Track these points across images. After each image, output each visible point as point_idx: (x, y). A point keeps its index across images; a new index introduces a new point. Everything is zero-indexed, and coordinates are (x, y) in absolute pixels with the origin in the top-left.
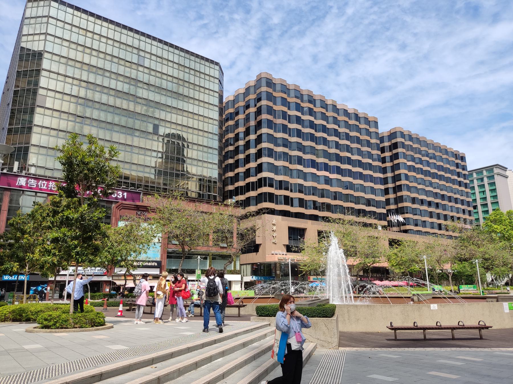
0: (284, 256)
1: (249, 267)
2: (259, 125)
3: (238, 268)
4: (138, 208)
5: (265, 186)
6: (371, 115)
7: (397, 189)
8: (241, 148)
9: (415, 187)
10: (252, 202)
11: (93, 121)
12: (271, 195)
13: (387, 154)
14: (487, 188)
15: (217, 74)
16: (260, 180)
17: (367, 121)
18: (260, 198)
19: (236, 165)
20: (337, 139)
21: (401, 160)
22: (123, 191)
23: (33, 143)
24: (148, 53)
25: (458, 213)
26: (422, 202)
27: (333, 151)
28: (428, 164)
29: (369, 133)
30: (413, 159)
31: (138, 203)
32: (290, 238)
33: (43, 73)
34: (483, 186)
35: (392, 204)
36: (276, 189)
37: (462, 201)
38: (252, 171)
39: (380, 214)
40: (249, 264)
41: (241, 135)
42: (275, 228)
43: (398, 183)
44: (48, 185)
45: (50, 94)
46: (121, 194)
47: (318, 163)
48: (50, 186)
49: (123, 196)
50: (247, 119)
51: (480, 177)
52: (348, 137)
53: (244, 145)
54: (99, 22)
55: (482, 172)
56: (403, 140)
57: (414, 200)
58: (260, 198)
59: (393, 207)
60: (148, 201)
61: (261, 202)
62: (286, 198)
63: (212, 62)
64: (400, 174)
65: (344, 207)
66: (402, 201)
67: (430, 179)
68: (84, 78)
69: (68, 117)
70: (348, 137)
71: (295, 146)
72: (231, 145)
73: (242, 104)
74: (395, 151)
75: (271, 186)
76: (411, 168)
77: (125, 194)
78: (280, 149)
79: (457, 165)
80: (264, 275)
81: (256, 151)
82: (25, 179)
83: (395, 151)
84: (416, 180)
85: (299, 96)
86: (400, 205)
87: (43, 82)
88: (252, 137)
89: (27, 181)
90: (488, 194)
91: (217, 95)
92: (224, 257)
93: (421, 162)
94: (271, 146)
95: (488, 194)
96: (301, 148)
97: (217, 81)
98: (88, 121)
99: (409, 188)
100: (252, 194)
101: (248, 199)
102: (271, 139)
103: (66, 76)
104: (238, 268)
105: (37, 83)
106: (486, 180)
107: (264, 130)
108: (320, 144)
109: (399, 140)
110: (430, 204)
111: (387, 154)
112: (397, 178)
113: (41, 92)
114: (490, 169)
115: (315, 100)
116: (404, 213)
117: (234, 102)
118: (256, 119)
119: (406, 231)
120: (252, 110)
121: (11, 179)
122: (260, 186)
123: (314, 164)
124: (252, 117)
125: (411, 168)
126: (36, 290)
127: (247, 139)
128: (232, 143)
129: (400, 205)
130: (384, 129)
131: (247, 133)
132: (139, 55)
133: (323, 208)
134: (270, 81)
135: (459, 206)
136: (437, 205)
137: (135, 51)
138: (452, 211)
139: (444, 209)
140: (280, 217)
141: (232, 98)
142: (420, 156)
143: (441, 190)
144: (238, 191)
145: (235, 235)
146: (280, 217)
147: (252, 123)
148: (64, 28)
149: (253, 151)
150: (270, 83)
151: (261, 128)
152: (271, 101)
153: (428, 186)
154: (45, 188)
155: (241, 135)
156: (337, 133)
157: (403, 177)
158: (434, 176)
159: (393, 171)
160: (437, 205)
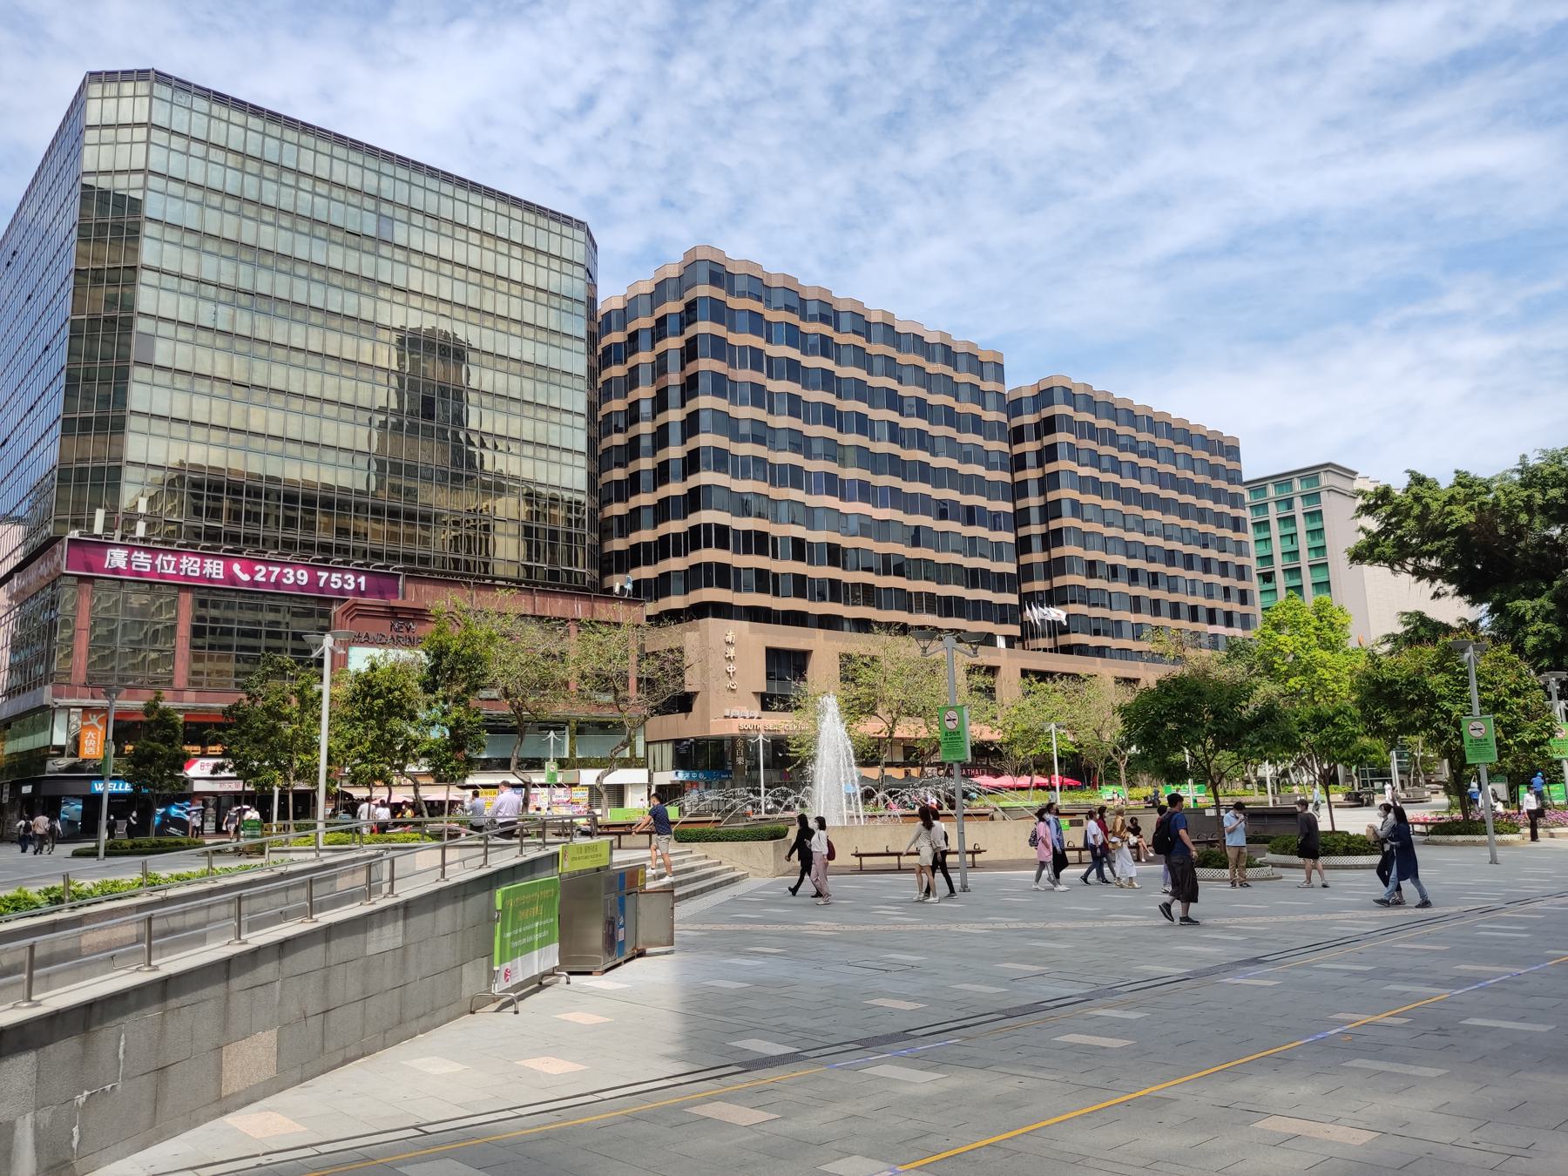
0: (755, 722)
1: (668, 750)
2: (690, 387)
3: (640, 753)
4: (393, 613)
5: (708, 545)
6: (984, 351)
7: (1053, 539)
8: (646, 443)
9: (1096, 530)
10: (675, 584)
11: (273, 395)
12: (723, 569)
13: (1030, 447)
14: (1302, 525)
15: (579, 252)
16: (695, 530)
17: (975, 363)
18: (697, 576)
19: (633, 484)
20: (893, 416)
21: (1063, 464)
22: (357, 573)
23: (130, 459)
24: (402, 206)
25: (1210, 596)
26: (1114, 571)
27: (884, 447)
28: (1136, 472)
29: (979, 396)
30: (1095, 460)
31: (398, 602)
32: (769, 676)
33: (146, 277)
34: (1291, 520)
35: (1039, 579)
36: (736, 551)
37: (1224, 565)
38: (675, 469)
39: (1003, 606)
40: (667, 741)
41: (646, 408)
42: (732, 652)
43: (1054, 524)
44: (178, 563)
45: (166, 329)
46: (351, 581)
47: (843, 481)
48: (183, 567)
49: (358, 585)
50: (660, 366)
51: (1286, 495)
52: (922, 409)
53: (653, 434)
54: (275, 130)
55: (1290, 483)
56: (1069, 410)
57: (1091, 568)
58: (697, 576)
59: (1039, 585)
60: (411, 595)
61: (697, 587)
62: (761, 574)
63: (567, 220)
64: (1059, 501)
65: (910, 594)
66: (1062, 572)
67: (1137, 510)
68: (245, 284)
69: (212, 387)
70: (922, 409)
71: (783, 439)
72: (619, 430)
73: (645, 322)
74: (1048, 440)
75: (723, 545)
76: (1085, 484)
77: (362, 580)
78: (746, 449)
79: (1214, 471)
80: (704, 768)
81: (682, 308)
82: (124, 553)
83: (1048, 440)
84: (1103, 516)
85: (796, 304)
86: (1058, 581)
87: (146, 299)
88: (675, 415)
89: (129, 557)
90: (1303, 542)
91: (582, 310)
92: (603, 727)
93: (1116, 466)
94: (722, 442)
95: (1303, 542)
96: (800, 443)
97: (580, 272)
98: (259, 396)
99: (1083, 539)
100: (675, 564)
101: (666, 576)
102: (727, 425)
103: (200, 281)
104: (640, 753)
105: (129, 306)
106: (1298, 504)
107: (705, 401)
108: (849, 431)
109: (1060, 409)
110: (1134, 576)
111: (1030, 447)
112: (1050, 511)
113: (142, 325)
114: (1310, 474)
115: (837, 313)
116: (1065, 603)
117: (625, 315)
118: (683, 368)
119: (1068, 649)
120: (674, 343)
121: (91, 554)
122: (696, 547)
123: (832, 485)
124: (674, 361)
125: (1085, 484)
126: (165, 816)
127: (661, 419)
128: (621, 425)
129: (1058, 581)
130: (1020, 380)
131: (660, 403)
132: (380, 215)
133: (855, 597)
134: (717, 270)
135: (1215, 578)
136: (1154, 580)
137: (369, 204)
138: (1193, 593)
139: (1172, 589)
140: (746, 624)
141: (619, 305)
142: (1113, 451)
143: (1167, 538)
144: (636, 556)
145: (633, 682)
146: (745, 625)
147: (674, 378)
148: (187, 153)
149: (675, 452)
150: (719, 275)
151: (696, 395)
152: (723, 323)
153: (1132, 530)
154: (171, 571)
155: (646, 408)
156: (894, 401)
157: (1066, 508)
158: (1147, 501)
159: (1042, 492)
160: (1154, 580)
